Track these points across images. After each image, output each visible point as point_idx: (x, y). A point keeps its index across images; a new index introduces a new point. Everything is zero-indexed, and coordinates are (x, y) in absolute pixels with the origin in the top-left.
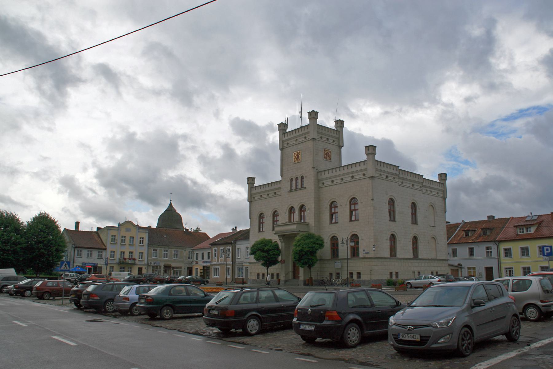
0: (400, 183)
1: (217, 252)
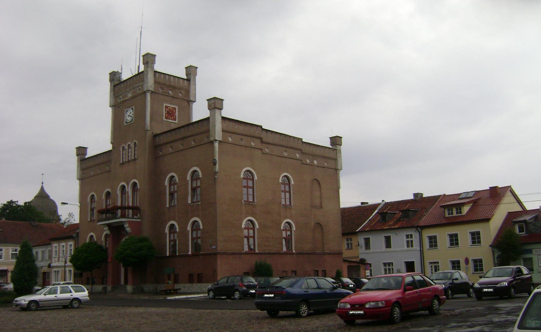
1: (65, 249)
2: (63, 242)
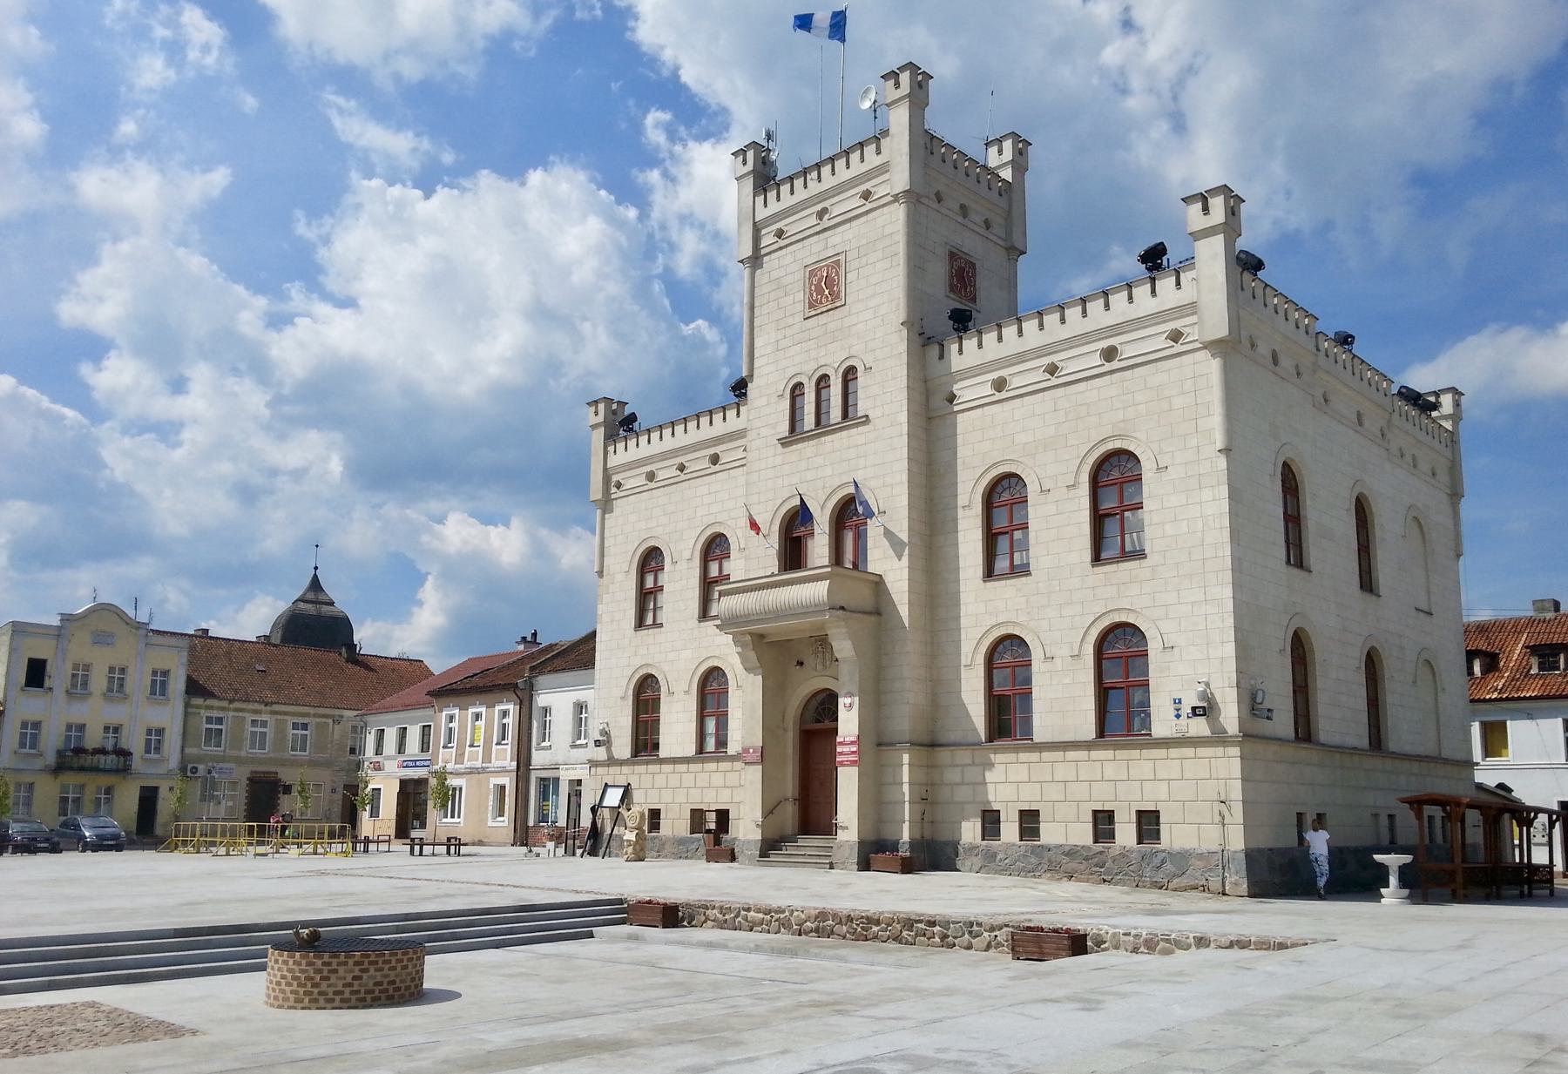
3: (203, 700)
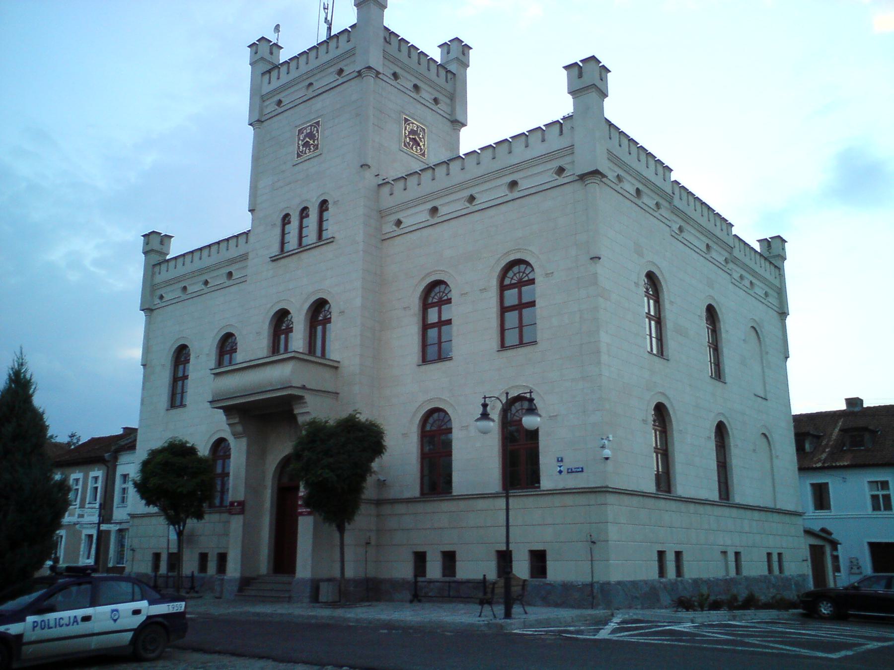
0: (675, 227)
2: (96, 469)
3: (839, 546)
